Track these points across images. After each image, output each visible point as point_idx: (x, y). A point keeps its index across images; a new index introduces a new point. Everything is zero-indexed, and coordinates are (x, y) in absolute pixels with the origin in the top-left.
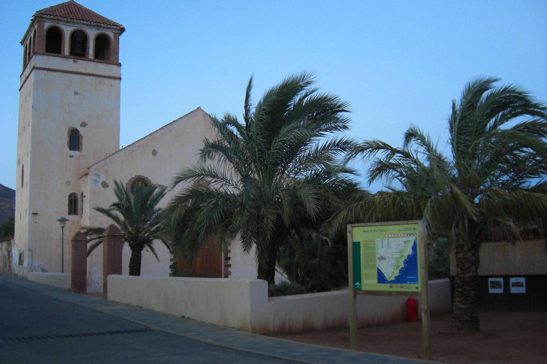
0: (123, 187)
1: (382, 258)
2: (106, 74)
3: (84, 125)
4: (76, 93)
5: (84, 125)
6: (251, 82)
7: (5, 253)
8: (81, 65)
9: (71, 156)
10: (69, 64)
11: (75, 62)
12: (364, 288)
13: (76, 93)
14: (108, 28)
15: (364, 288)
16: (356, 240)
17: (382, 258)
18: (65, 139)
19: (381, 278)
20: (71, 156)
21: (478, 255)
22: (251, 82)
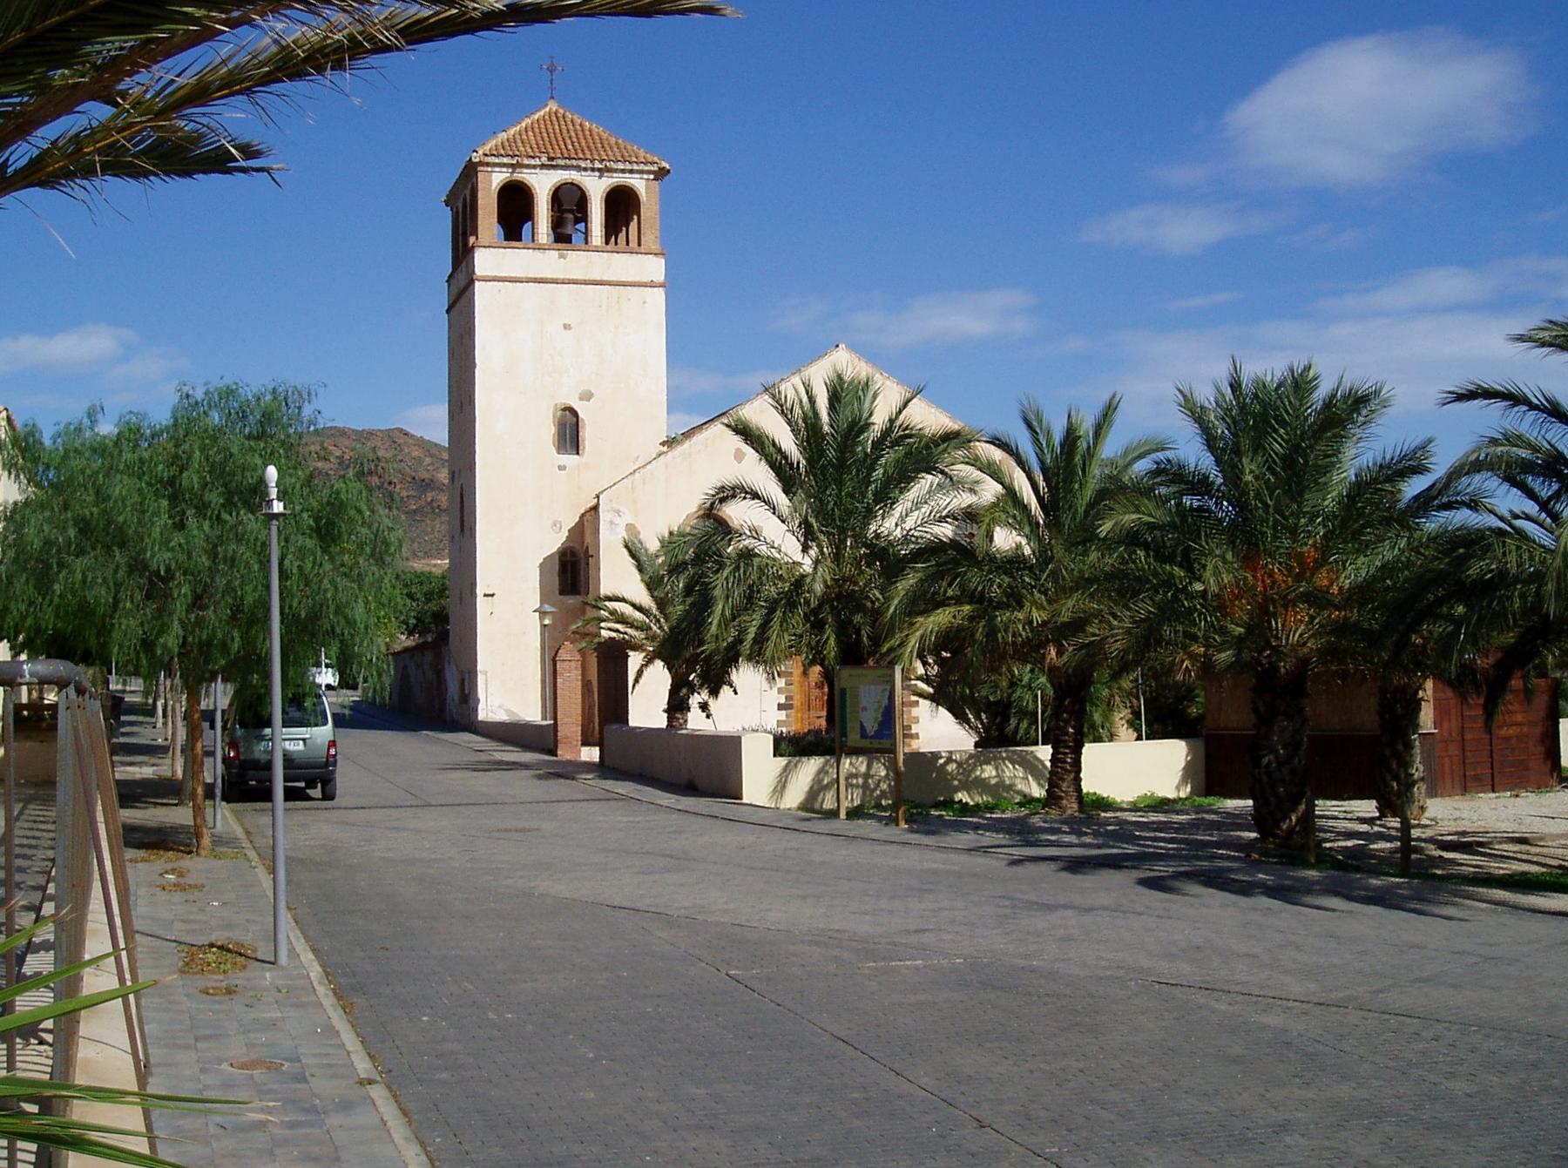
0: (201, 94)
1: (864, 709)
2: (630, 279)
3: (587, 396)
4: (567, 327)
5: (587, 396)
6: (1461, 397)
7: (430, 674)
8: (576, 262)
9: (562, 468)
10: (550, 262)
11: (561, 256)
12: (850, 744)
13: (567, 327)
14: (631, 171)
15: (850, 744)
16: (844, 685)
17: (864, 709)
18: (549, 431)
19: (864, 735)
20: (562, 468)
21: (147, 174)
22: (1461, 397)
